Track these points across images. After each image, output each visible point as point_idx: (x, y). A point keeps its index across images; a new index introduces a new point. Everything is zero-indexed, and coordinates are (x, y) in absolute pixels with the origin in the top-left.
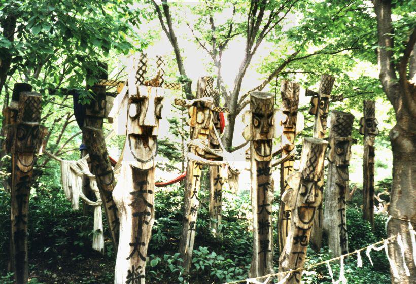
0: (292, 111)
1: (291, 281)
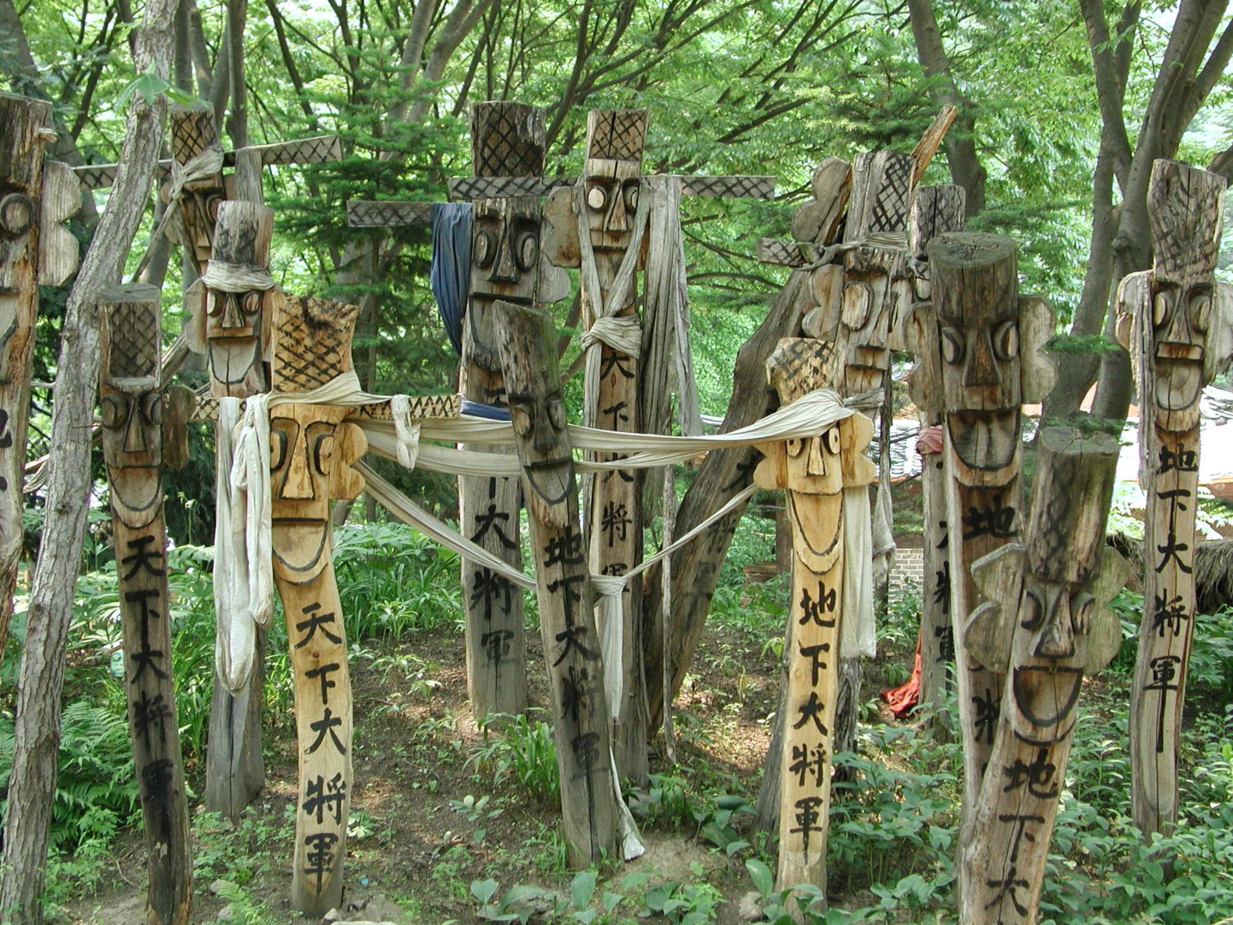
0: (1187, 282)
1: (997, 907)
